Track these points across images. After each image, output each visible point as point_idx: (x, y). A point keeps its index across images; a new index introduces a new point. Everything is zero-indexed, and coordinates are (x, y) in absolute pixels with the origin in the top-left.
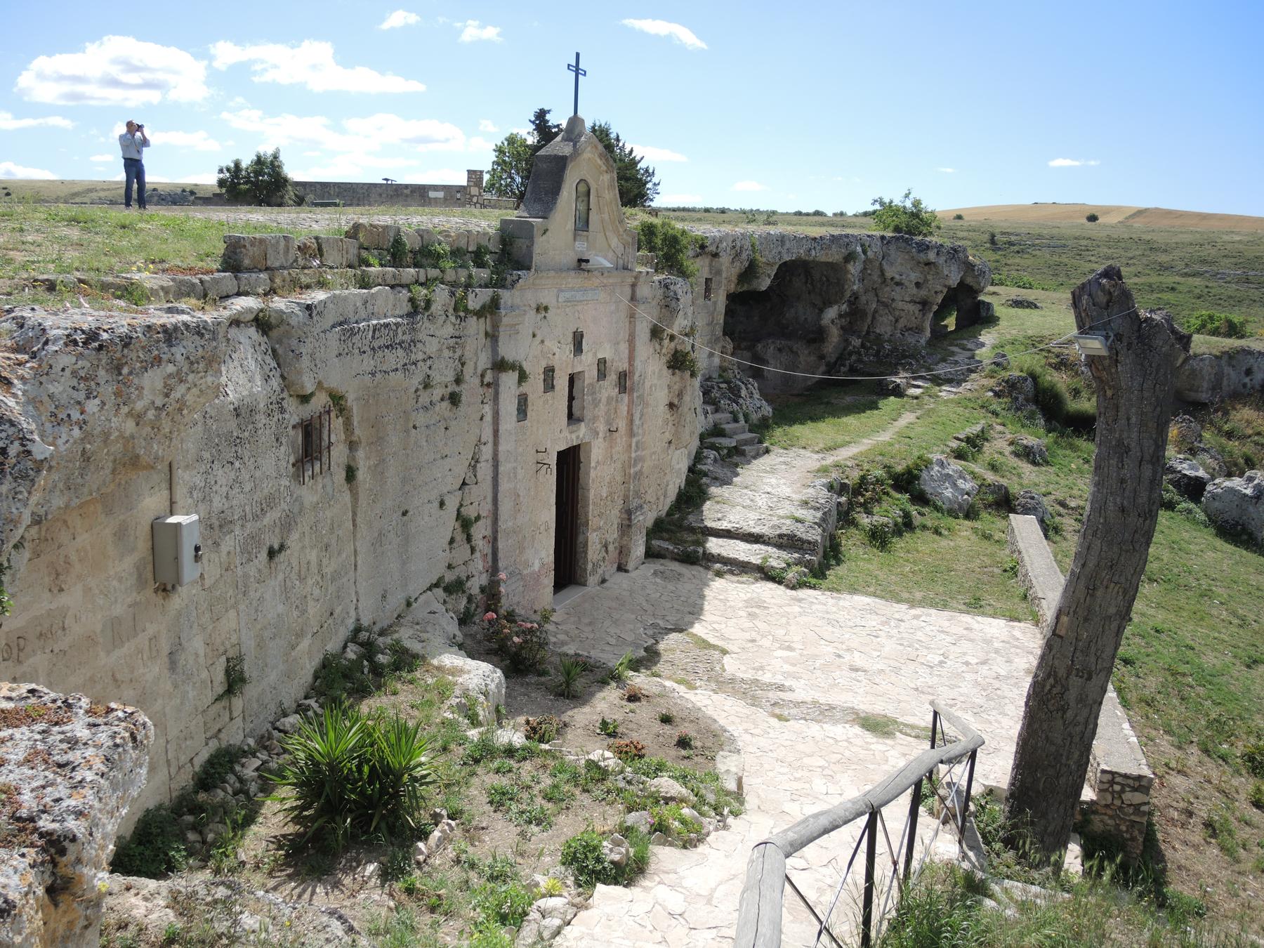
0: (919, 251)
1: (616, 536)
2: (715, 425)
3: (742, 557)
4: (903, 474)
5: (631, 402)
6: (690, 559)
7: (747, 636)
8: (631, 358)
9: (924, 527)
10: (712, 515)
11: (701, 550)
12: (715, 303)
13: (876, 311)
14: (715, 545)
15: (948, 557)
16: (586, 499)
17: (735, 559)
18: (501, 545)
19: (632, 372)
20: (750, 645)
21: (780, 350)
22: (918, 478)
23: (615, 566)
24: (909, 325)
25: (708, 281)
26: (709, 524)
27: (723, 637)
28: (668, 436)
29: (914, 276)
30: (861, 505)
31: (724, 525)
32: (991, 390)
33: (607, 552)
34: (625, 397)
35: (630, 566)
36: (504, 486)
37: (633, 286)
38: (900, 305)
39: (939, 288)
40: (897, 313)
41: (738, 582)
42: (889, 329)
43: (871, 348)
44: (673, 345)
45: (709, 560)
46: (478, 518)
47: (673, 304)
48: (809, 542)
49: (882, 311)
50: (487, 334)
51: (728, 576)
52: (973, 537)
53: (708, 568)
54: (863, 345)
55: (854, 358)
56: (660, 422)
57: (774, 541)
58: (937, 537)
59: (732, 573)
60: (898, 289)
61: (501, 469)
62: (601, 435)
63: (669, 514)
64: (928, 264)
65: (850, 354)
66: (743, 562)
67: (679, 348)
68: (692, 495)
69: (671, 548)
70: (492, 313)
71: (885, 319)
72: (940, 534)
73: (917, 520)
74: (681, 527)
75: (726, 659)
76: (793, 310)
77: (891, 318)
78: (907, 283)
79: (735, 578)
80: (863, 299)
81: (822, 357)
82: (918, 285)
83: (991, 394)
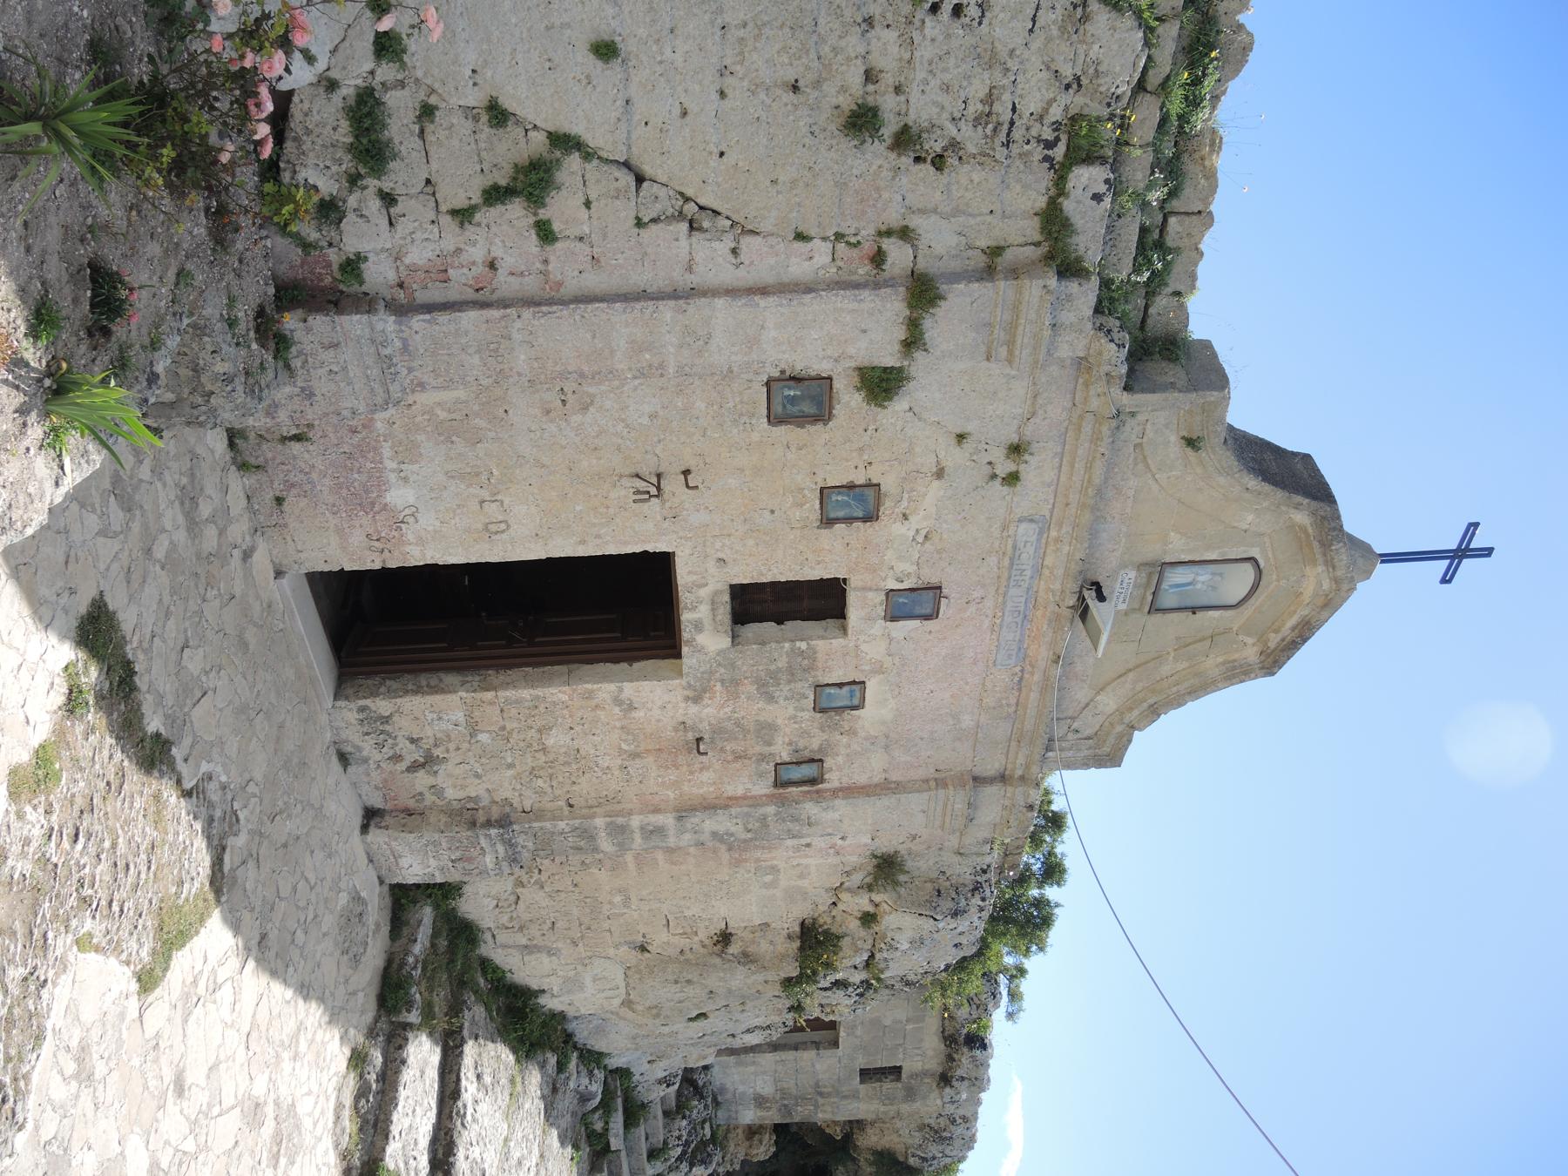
1: (451, 794)
2: (643, 1106)
3: (400, 1121)
5: (754, 801)
6: (391, 991)
7: (195, 1076)
8: (849, 791)
10: (488, 1060)
11: (414, 1017)
12: (855, 1096)
14: (423, 1054)
16: (548, 681)
17: (394, 1102)
18: (470, 317)
19: (819, 797)
20: (169, 1076)
23: (377, 802)
25: (897, 1071)
26: (470, 1049)
27: (190, 1002)
28: (660, 940)
31: (469, 1088)
33: (414, 767)
34: (763, 787)
35: (377, 837)
36: (622, 324)
37: (1003, 778)
41: (339, 1106)
44: (853, 924)
45: (391, 1037)
46: (545, 233)
47: (947, 905)
50: (996, 251)
51: (352, 1083)
53: (371, 1033)
56: (694, 910)
59: (361, 1094)
61: (667, 310)
62: (693, 709)
63: (485, 964)
66: (388, 1121)
67: (845, 943)
68: (529, 1025)
69: (417, 949)
70: (1049, 257)
74: (461, 984)
75: (122, 979)
79: (348, 1101)
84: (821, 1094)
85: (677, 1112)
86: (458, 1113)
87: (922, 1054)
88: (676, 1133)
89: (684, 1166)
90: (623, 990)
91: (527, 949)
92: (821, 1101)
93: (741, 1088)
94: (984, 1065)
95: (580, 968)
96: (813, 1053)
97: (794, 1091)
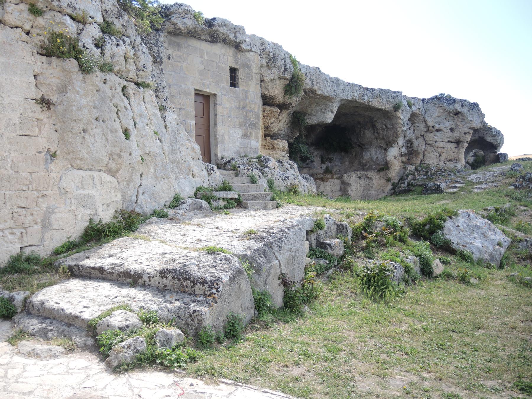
0: (449, 105)
4: (425, 225)
9: (448, 276)
12: (246, 92)
13: (425, 151)
15: (475, 308)
21: (360, 177)
22: (441, 228)
24: (449, 158)
29: (449, 124)
30: (363, 249)
32: (513, 185)
38: (442, 144)
39: (467, 130)
40: (440, 150)
42: (435, 161)
43: (421, 170)
48: (203, 282)
49: (429, 149)
52: (510, 286)
54: (416, 169)
55: (410, 177)
57: (155, 282)
58: (463, 287)
60: (438, 134)
64: (457, 113)
65: (407, 175)
71: (431, 155)
72: (468, 283)
73: (438, 267)
76: (368, 154)
77: (436, 154)
78: (444, 130)
80: (416, 144)
81: (389, 180)
82: (452, 130)
83: (512, 187)
84: (244, 108)
85: (237, 170)
86: (112, 268)
87: (225, 57)
88: (246, 171)
89: (266, 170)
90: (96, 174)
91: (46, 225)
92: (248, 108)
93: (238, 144)
94: (220, 19)
95: (69, 196)
96: (218, 107)
97: (241, 120)
